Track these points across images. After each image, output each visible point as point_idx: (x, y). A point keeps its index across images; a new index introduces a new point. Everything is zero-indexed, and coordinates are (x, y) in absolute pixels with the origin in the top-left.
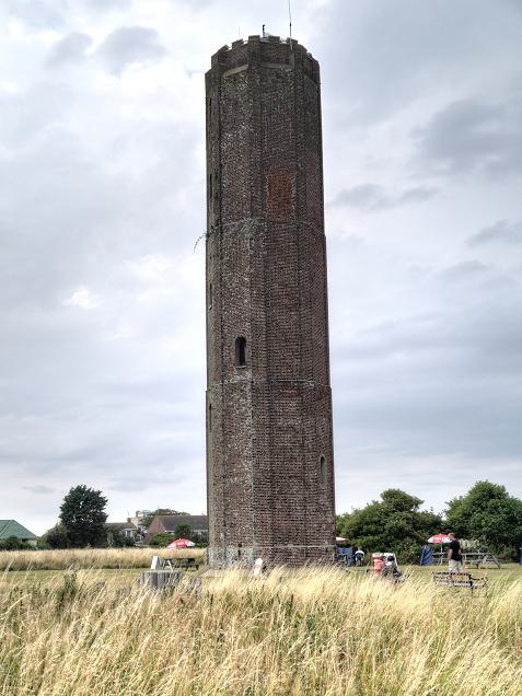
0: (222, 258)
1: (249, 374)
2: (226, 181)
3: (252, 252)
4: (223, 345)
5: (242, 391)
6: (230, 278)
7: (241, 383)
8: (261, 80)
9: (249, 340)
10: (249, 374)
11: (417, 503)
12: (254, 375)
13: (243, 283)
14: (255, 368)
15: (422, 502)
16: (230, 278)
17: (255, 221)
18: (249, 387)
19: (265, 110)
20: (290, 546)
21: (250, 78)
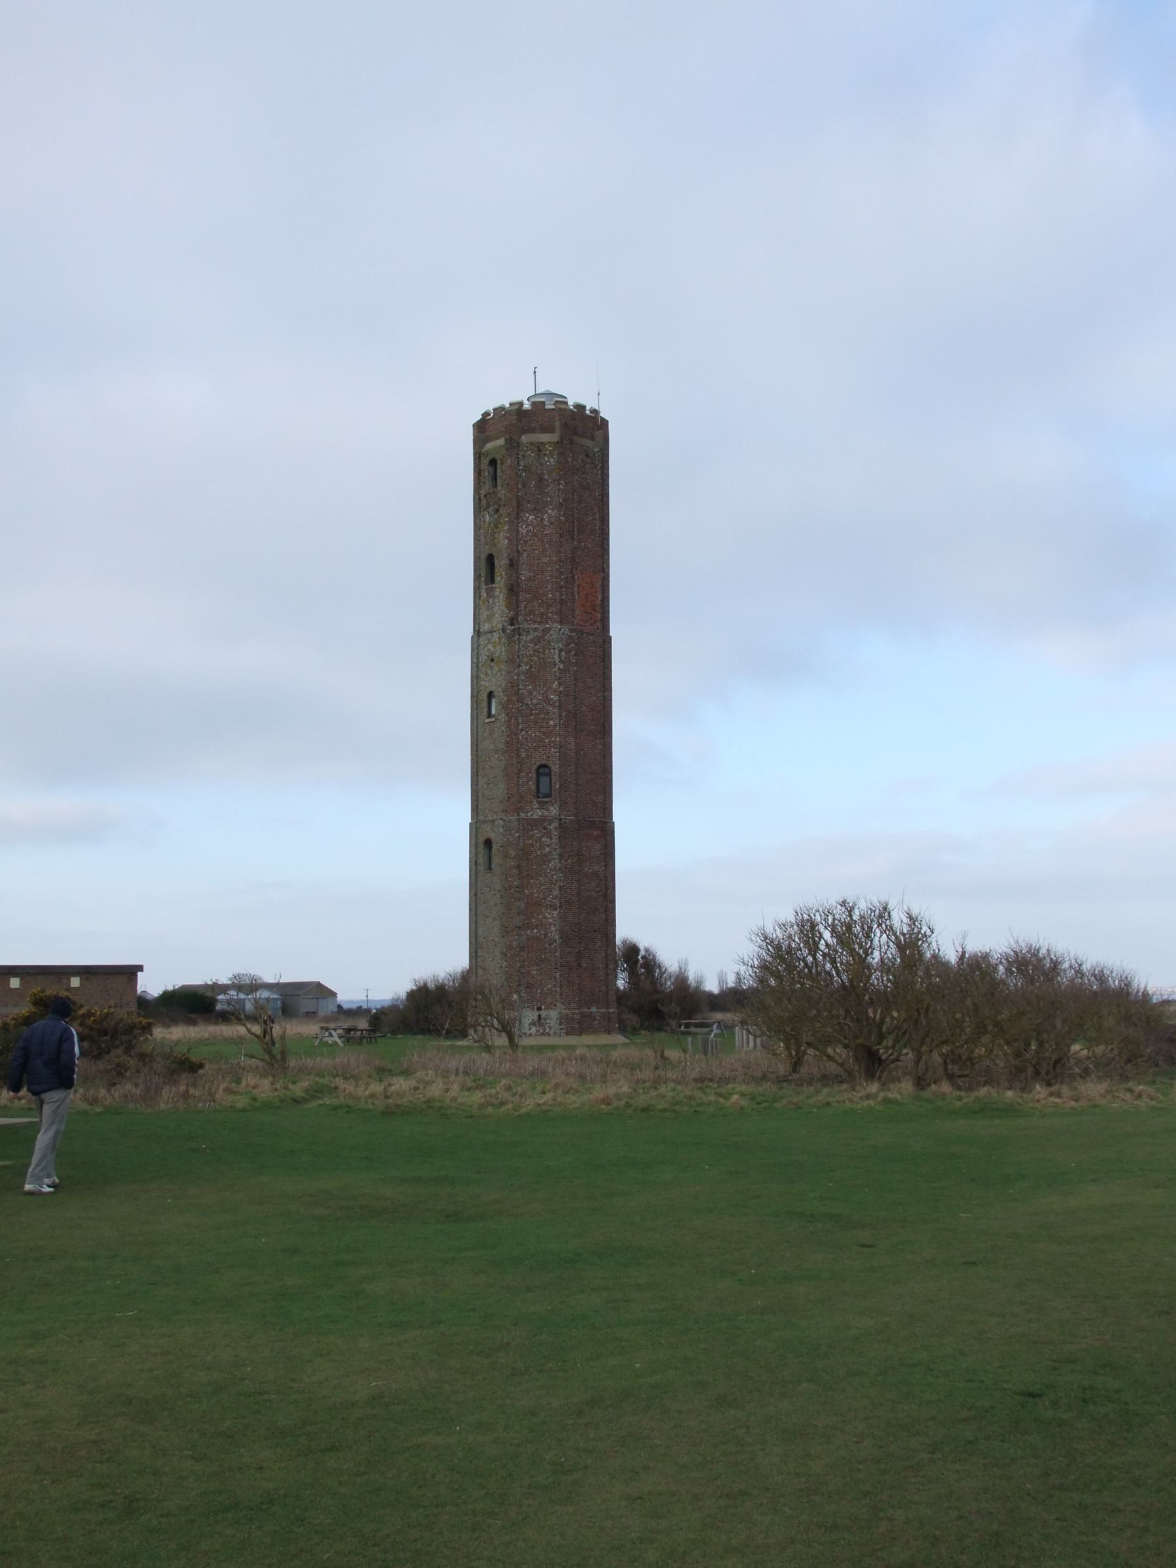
0: (519, 666)
1: (554, 810)
2: (525, 574)
3: (562, 666)
4: (520, 771)
5: (545, 828)
6: (530, 693)
7: (543, 819)
8: (573, 459)
9: (555, 768)
10: (554, 810)
11: (130, 973)
12: (561, 810)
13: (548, 701)
14: (563, 805)
15: (140, 968)
16: (530, 693)
17: (566, 629)
18: (556, 824)
19: (543, 486)
20: (593, 1009)
21: (560, 454)
